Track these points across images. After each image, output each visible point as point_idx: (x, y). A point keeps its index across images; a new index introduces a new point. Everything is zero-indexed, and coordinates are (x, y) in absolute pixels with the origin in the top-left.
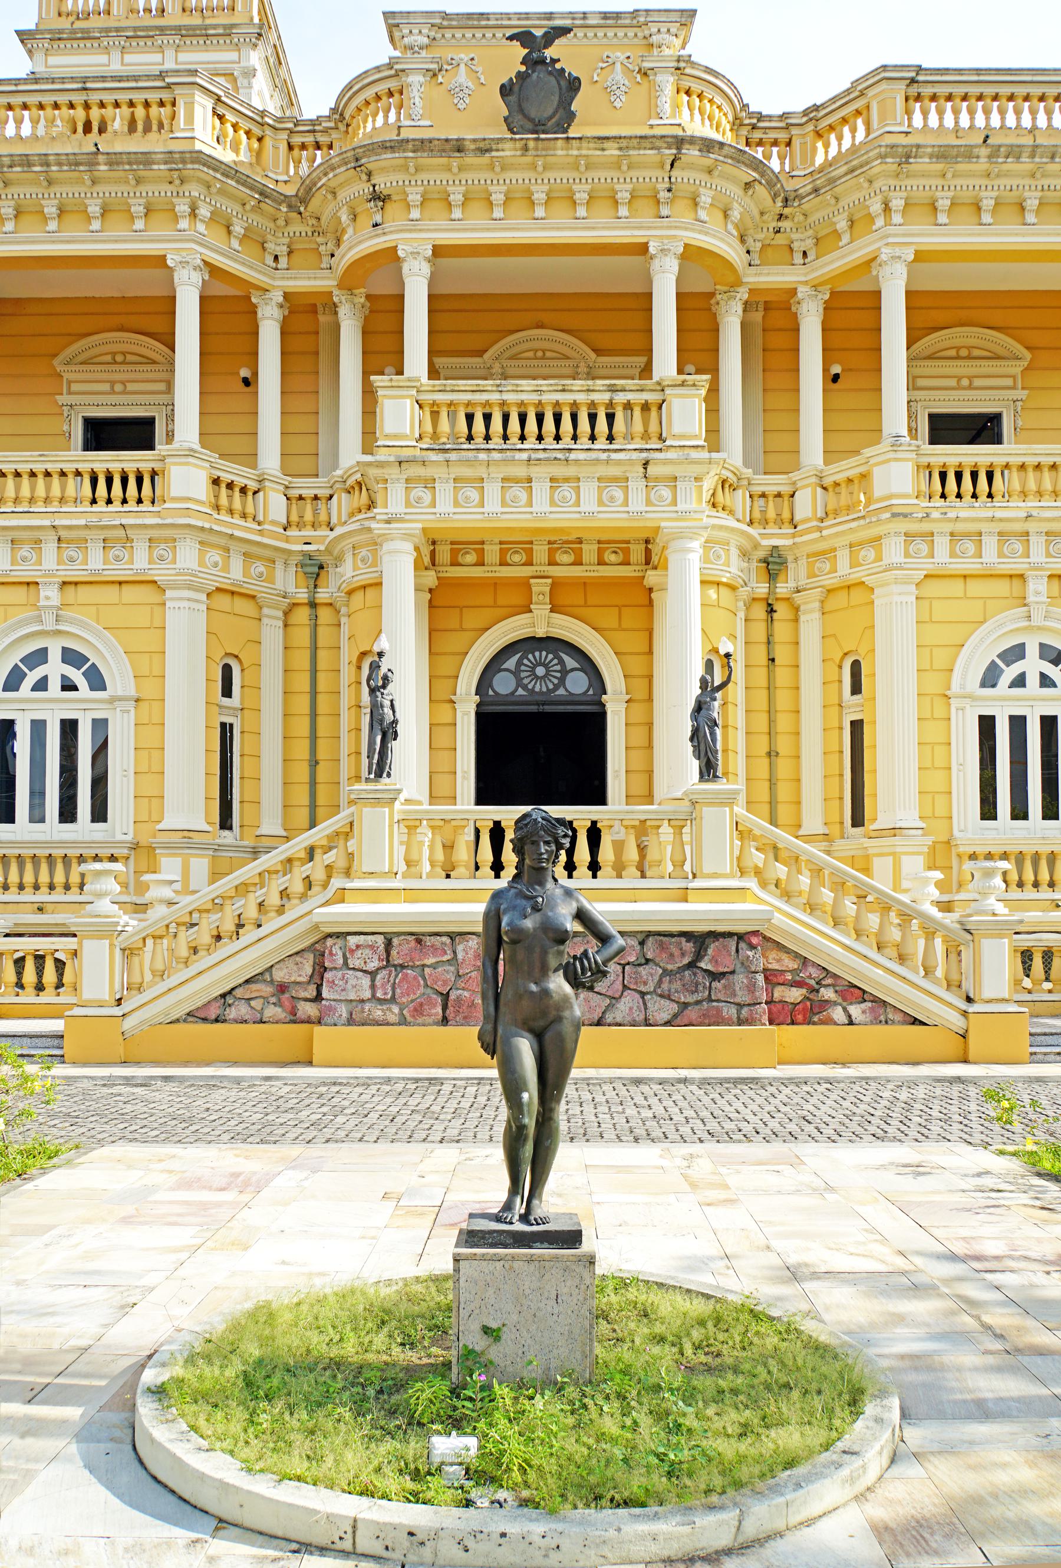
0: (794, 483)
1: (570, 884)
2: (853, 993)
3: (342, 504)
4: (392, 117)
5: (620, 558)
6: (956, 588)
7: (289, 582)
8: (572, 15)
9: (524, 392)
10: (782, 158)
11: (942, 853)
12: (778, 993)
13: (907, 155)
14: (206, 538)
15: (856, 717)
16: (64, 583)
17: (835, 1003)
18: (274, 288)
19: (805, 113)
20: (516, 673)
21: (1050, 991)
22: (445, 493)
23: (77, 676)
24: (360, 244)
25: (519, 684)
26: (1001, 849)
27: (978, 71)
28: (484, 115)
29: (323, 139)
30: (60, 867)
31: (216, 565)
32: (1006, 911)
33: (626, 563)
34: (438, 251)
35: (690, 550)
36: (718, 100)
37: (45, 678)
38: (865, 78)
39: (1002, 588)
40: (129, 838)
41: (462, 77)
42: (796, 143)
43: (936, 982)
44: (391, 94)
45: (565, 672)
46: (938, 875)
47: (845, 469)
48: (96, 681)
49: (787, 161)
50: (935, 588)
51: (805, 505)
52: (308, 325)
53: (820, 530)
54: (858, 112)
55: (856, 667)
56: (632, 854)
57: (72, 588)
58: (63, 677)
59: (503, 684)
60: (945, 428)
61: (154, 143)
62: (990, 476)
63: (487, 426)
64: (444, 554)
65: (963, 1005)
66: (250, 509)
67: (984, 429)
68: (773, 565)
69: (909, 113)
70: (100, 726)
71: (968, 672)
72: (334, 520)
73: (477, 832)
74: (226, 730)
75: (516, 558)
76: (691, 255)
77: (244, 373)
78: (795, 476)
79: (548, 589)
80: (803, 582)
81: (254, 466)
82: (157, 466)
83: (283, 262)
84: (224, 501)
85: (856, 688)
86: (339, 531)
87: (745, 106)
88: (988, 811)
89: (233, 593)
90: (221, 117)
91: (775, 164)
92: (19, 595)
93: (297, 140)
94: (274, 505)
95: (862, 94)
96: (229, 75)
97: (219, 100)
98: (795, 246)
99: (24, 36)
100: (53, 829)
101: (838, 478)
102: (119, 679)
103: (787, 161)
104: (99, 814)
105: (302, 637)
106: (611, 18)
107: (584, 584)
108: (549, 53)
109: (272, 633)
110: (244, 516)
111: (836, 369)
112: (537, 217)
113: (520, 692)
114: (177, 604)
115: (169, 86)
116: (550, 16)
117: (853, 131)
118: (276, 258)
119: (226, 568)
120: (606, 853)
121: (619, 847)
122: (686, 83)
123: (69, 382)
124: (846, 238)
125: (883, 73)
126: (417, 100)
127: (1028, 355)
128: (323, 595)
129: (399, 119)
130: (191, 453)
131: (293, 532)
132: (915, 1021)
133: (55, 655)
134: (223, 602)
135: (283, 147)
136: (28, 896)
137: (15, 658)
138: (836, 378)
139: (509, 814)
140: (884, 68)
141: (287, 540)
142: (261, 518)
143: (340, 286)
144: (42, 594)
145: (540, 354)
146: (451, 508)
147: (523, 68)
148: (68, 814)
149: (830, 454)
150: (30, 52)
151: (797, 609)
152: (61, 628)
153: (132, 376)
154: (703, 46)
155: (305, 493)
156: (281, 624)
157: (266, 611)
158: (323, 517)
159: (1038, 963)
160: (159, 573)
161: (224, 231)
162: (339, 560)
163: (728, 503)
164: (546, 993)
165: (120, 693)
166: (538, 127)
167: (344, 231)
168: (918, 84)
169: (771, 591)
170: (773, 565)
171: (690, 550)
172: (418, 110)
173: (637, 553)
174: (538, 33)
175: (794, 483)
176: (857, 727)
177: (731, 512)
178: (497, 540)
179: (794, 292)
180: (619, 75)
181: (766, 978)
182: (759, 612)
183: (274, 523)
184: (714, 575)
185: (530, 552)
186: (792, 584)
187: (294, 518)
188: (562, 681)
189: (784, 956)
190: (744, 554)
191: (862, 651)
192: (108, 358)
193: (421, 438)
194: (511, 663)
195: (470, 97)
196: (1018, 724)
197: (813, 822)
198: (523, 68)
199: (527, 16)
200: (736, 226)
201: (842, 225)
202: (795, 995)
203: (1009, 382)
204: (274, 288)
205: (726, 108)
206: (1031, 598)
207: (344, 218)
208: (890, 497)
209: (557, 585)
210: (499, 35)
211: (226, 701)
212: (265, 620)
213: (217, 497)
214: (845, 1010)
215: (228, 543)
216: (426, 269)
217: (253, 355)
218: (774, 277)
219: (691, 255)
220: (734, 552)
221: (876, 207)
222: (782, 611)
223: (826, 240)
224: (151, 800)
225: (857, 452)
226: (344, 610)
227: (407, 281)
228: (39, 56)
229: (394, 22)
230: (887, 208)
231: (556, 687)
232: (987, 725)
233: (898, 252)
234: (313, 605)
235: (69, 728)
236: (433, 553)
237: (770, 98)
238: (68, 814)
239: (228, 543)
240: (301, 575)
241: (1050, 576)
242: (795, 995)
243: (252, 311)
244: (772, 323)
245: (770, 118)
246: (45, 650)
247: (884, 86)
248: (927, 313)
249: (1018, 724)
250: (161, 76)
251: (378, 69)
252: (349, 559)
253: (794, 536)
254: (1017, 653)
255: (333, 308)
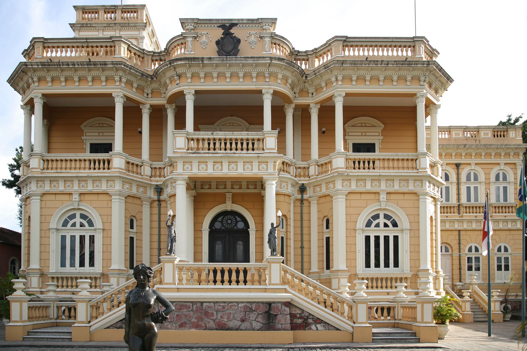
0: (309, 164)
1: (396, 284)
2: (318, 321)
3: (168, 169)
4: (183, 51)
5: (238, 187)
6: (358, 196)
7: (152, 194)
8: (239, 20)
9: (401, 155)
10: (306, 64)
11: (353, 277)
12: (295, 321)
13: (343, 62)
14: (125, 181)
15: (328, 236)
16: (81, 194)
17: (313, 324)
18: (147, 103)
19: (312, 51)
20: (222, 222)
21: (383, 320)
22: (195, 165)
23: (85, 222)
24: (173, 89)
25: (223, 225)
26: (366, 277)
27: (393, 38)
28: (211, 51)
29: (163, 58)
30: (70, 281)
31: (128, 188)
32: (366, 296)
33: (255, 188)
34: (197, 92)
35: (273, 184)
36: (285, 46)
37: (379, 223)
38: (330, 40)
39: (372, 196)
40: (101, 271)
41: (204, 39)
42: (310, 60)
43: (345, 317)
44: (182, 44)
45: (237, 222)
46: (349, 284)
47: (324, 160)
48: (91, 224)
49: (307, 65)
50: (352, 197)
51: (313, 170)
52: (158, 115)
53: (317, 178)
54: (328, 51)
55: (328, 221)
56: (256, 277)
57: (83, 195)
58: (81, 222)
59: (218, 225)
60: (358, 148)
61: (109, 59)
62: (374, 162)
63: (236, 146)
64: (199, 185)
65: (352, 324)
66: (139, 171)
67: (370, 148)
68: (302, 189)
69: (344, 50)
70: (396, 238)
71: (361, 223)
72: (166, 175)
73: (209, 270)
74: (132, 239)
75: (221, 187)
76: (276, 94)
77: (139, 130)
78: (309, 162)
79: (231, 196)
80: (312, 194)
81: (141, 158)
82: (109, 158)
83: (150, 96)
84: (131, 169)
85: (327, 227)
86: (167, 178)
87: (293, 48)
88: (368, 265)
89: (133, 197)
90: (130, 51)
91: (303, 67)
92: (67, 197)
93: (154, 58)
94: (147, 170)
95: (330, 45)
96: (136, 39)
97: (129, 45)
98: (309, 91)
99: (72, 25)
100: (77, 269)
101: (322, 162)
102: (98, 224)
103: (307, 65)
104: (92, 264)
105: (156, 210)
106: (251, 22)
107: (242, 195)
108: (232, 31)
109: (146, 210)
110: (137, 174)
111: (324, 129)
112: (227, 81)
113: (223, 228)
114: (115, 200)
115: (113, 41)
116: (231, 20)
117: (327, 56)
118: (148, 94)
119: (131, 189)
120: (249, 277)
121: (253, 275)
122: (274, 41)
123: (86, 133)
124: (325, 89)
125: (336, 39)
126: (190, 46)
127: (383, 126)
128: (162, 198)
129: (185, 52)
130: (119, 154)
131: (153, 179)
132: (338, 329)
133: (382, 216)
134: (130, 200)
135: (150, 60)
136: (69, 289)
137: (369, 217)
138: (324, 132)
139: (219, 265)
140: (336, 37)
141: (151, 181)
142: (142, 174)
143: (168, 103)
144: (74, 197)
145: (232, 124)
146: (198, 171)
147: (223, 36)
148: (82, 264)
149: (320, 155)
150: (74, 30)
151: (310, 203)
152: (80, 207)
153: (104, 131)
154: (279, 30)
155: (156, 166)
156: (149, 207)
157: (144, 203)
158: (162, 174)
159: (385, 311)
160: (110, 190)
161: (131, 86)
162: (167, 186)
163: (288, 170)
164: (144, 324)
165: (98, 228)
166: (228, 54)
167: (168, 86)
168: (347, 42)
169: (302, 196)
170: (302, 189)
171: (273, 184)
172: (190, 50)
173: (259, 186)
174: (228, 25)
175: (309, 164)
176: (328, 239)
177: (289, 173)
178: (215, 181)
179: (309, 105)
180: (253, 38)
181: (290, 316)
182: (298, 204)
183: (146, 176)
184: (284, 191)
185: (225, 185)
186: (308, 195)
187: (153, 174)
188: (236, 225)
189: (297, 309)
190: (293, 186)
191: (329, 216)
192: (98, 125)
193: (188, 149)
194: (220, 219)
195: (207, 46)
196: (386, 238)
197: (315, 268)
198: (223, 36)
199: (225, 20)
200: (290, 85)
201: (323, 84)
202: (300, 321)
203: (377, 134)
204: (147, 103)
205: (287, 49)
206: (381, 200)
207: (168, 82)
208: (338, 168)
209: (234, 195)
210: (216, 26)
211: (132, 230)
212: (144, 206)
213: (128, 168)
214: (315, 326)
215: (130, 182)
216: (193, 98)
217: (140, 125)
218: (302, 101)
219: (276, 94)
220: (290, 186)
221: (333, 79)
222: (306, 203)
223: (318, 89)
224: (107, 260)
225: (328, 155)
226: (169, 202)
227: (187, 101)
228: (77, 32)
229: (183, 22)
230: (337, 80)
231: (234, 226)
232: (368, 238)
233: (340, 93)
234: (159, 201)
235: (82, 238)
236: (195, 185)
237: (301, 46)
238: (82, 264)
239: (130, 182)
240: (155, 192)
241: (387, 193)
242: (300, 321)
243: (140, 110)
244: (303, 115)
245: (302, 52)
246: (75, 214)
247: (336, 42)
248: (350, 113)
249: (377, 238)
250: (111, 38)
251: (178, 36)
252: (169, 187)
253: (309, 180)
254: (376, 217)
255: (166, 110)
